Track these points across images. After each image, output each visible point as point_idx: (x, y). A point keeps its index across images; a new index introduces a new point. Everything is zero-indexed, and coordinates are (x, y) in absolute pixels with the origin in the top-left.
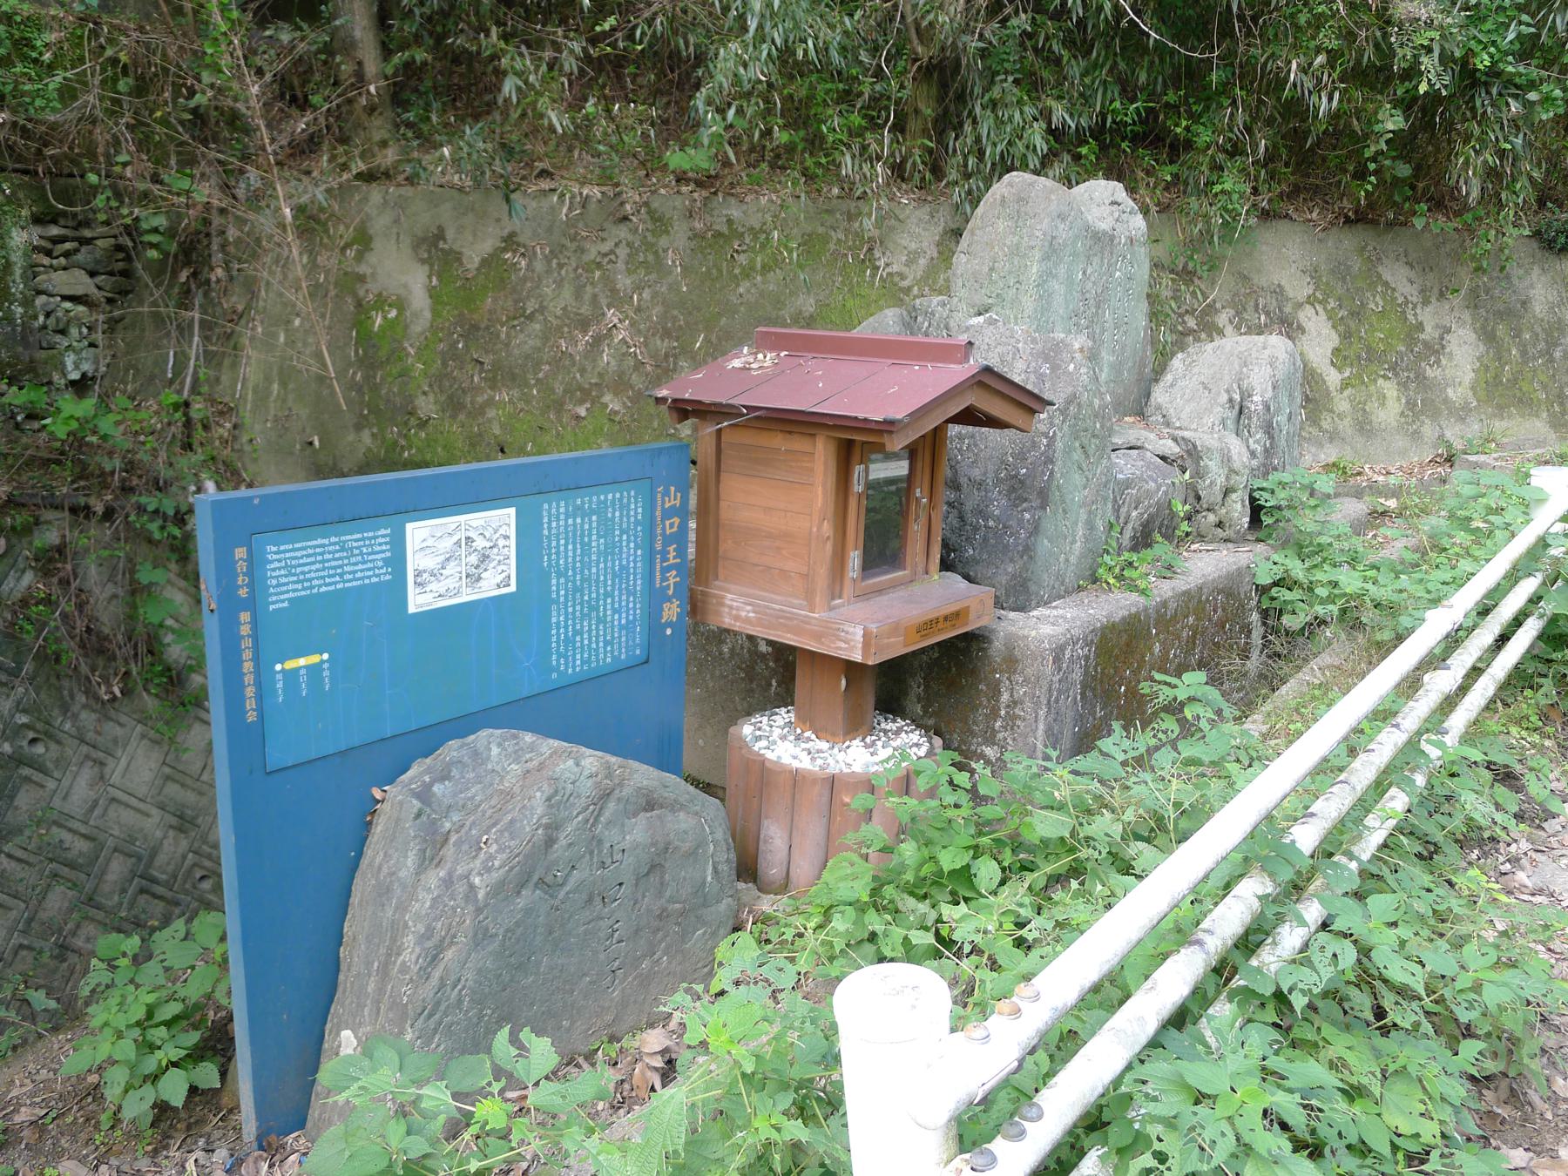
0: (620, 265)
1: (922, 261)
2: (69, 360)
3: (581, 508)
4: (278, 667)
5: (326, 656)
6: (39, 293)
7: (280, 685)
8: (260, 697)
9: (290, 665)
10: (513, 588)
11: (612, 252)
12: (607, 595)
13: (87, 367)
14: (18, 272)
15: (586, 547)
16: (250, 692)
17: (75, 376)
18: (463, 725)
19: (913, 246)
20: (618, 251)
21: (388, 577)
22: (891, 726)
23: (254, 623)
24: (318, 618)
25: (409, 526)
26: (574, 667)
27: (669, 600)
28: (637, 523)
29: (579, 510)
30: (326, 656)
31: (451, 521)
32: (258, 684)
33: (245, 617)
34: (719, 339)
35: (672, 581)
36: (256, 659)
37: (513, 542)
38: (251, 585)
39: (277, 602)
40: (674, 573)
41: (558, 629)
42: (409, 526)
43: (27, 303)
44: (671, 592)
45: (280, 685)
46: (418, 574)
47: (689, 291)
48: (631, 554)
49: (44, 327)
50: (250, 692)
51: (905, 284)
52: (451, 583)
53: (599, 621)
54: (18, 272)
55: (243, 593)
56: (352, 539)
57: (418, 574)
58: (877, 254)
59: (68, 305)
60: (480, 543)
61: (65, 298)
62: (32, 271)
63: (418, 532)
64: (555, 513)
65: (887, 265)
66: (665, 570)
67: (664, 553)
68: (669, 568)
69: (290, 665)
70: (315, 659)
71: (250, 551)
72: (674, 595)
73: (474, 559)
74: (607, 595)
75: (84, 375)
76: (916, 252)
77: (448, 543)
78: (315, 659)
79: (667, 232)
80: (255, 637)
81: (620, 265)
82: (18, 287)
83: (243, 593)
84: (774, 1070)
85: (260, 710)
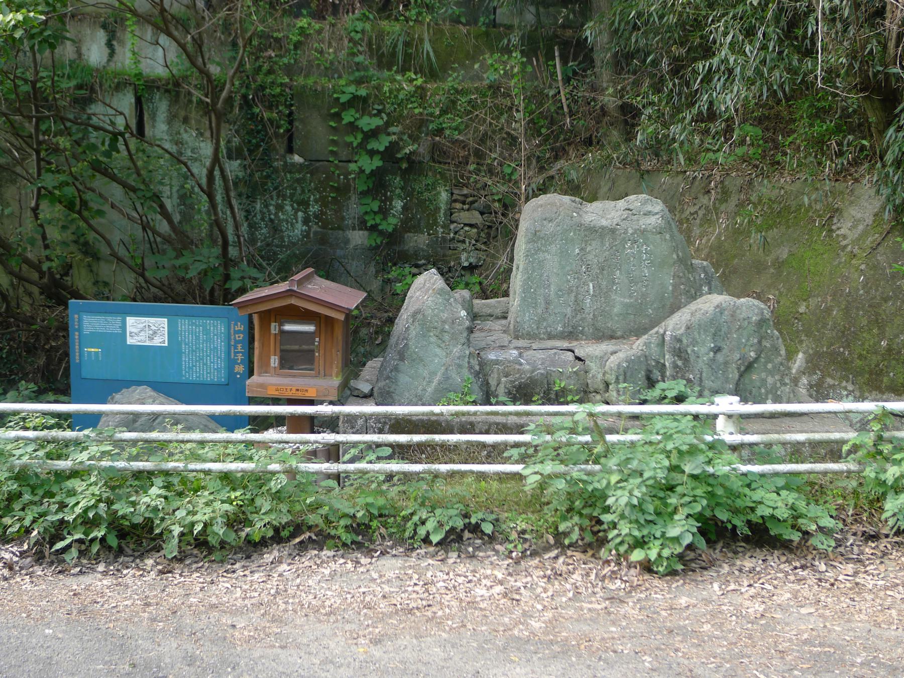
0: (698, 221)
1: (861, 227)
2: (464, 256)
3: (195, 323)
6: (452, 222)
8: (80, 356)
10: (166, 344)
11: (696, 212)
12: (207, 356)
13: (472, 260)
14: (442, 211)
15: (198, 338)
16: (77, 354)
17: (466, 264)
18: (139, 383)
19: (859, 216)
20: (699, 212)
22: (748, 564)
23: (79, 336)
24: (97, 339)
25: (128, 318)
28: (221, 333)
29: (193, 324)
31: (143, 319)
32: (80, 352)
33: (77, 333)
34: (730, 272)
36: (80, 346)
37: (166, 329)
38: (79, 325)
39: (86, 332)
43: (444, 226)
46: (131, 333)
47: (725, 240)
48: (220, 344)
49: (454, 238)
50: (77, 354)
51: (844, 243)
52: (143, 338)
53: (204, 364)
54: (442, 211)
56: (109, 318)
57: (131, 333)
58: (835, 220)
59: (467, 228)
60: (153, 328)
61: (466, 225)
62: (450, 212)
63: (130, 320)
64: (184, 324)
65: (838, 229)
66: (236, 353)
67: (236, 348)
73: (151, 332)
74: (207, 356)
75: (471, 264)
76: (859, 220)
77: (141, 326)
79: (726, 201)
80: (79, 339)
81: (698, 221)
82: (441, 218)
84: (320, 621)
85: (80, 359)
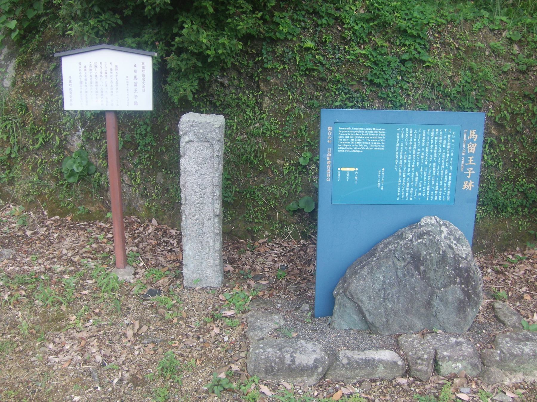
4: (339, 169)
5: (357, 169)
7: (339, 175)
9: (343, 169)
21: (383, 149)
25: (68, 106)
26: (446, 198)
27: (468, 180)
30: (357, 169)
35: (470, 172)
40: (472, 169)
41: (402, 180)
42: (68, 106)
44: (469, 177)
45: (339, 175)
55: (329, 142)
68: (470, 166)
69: (343, 169)
70: (353, 169)
71: (334, 128)
72: (470, 179)
78: (353, 169)
83: (329, 142)
